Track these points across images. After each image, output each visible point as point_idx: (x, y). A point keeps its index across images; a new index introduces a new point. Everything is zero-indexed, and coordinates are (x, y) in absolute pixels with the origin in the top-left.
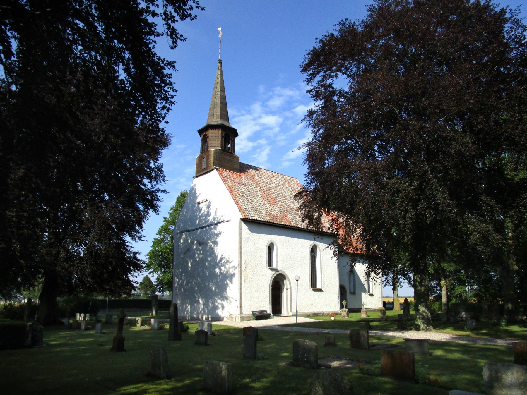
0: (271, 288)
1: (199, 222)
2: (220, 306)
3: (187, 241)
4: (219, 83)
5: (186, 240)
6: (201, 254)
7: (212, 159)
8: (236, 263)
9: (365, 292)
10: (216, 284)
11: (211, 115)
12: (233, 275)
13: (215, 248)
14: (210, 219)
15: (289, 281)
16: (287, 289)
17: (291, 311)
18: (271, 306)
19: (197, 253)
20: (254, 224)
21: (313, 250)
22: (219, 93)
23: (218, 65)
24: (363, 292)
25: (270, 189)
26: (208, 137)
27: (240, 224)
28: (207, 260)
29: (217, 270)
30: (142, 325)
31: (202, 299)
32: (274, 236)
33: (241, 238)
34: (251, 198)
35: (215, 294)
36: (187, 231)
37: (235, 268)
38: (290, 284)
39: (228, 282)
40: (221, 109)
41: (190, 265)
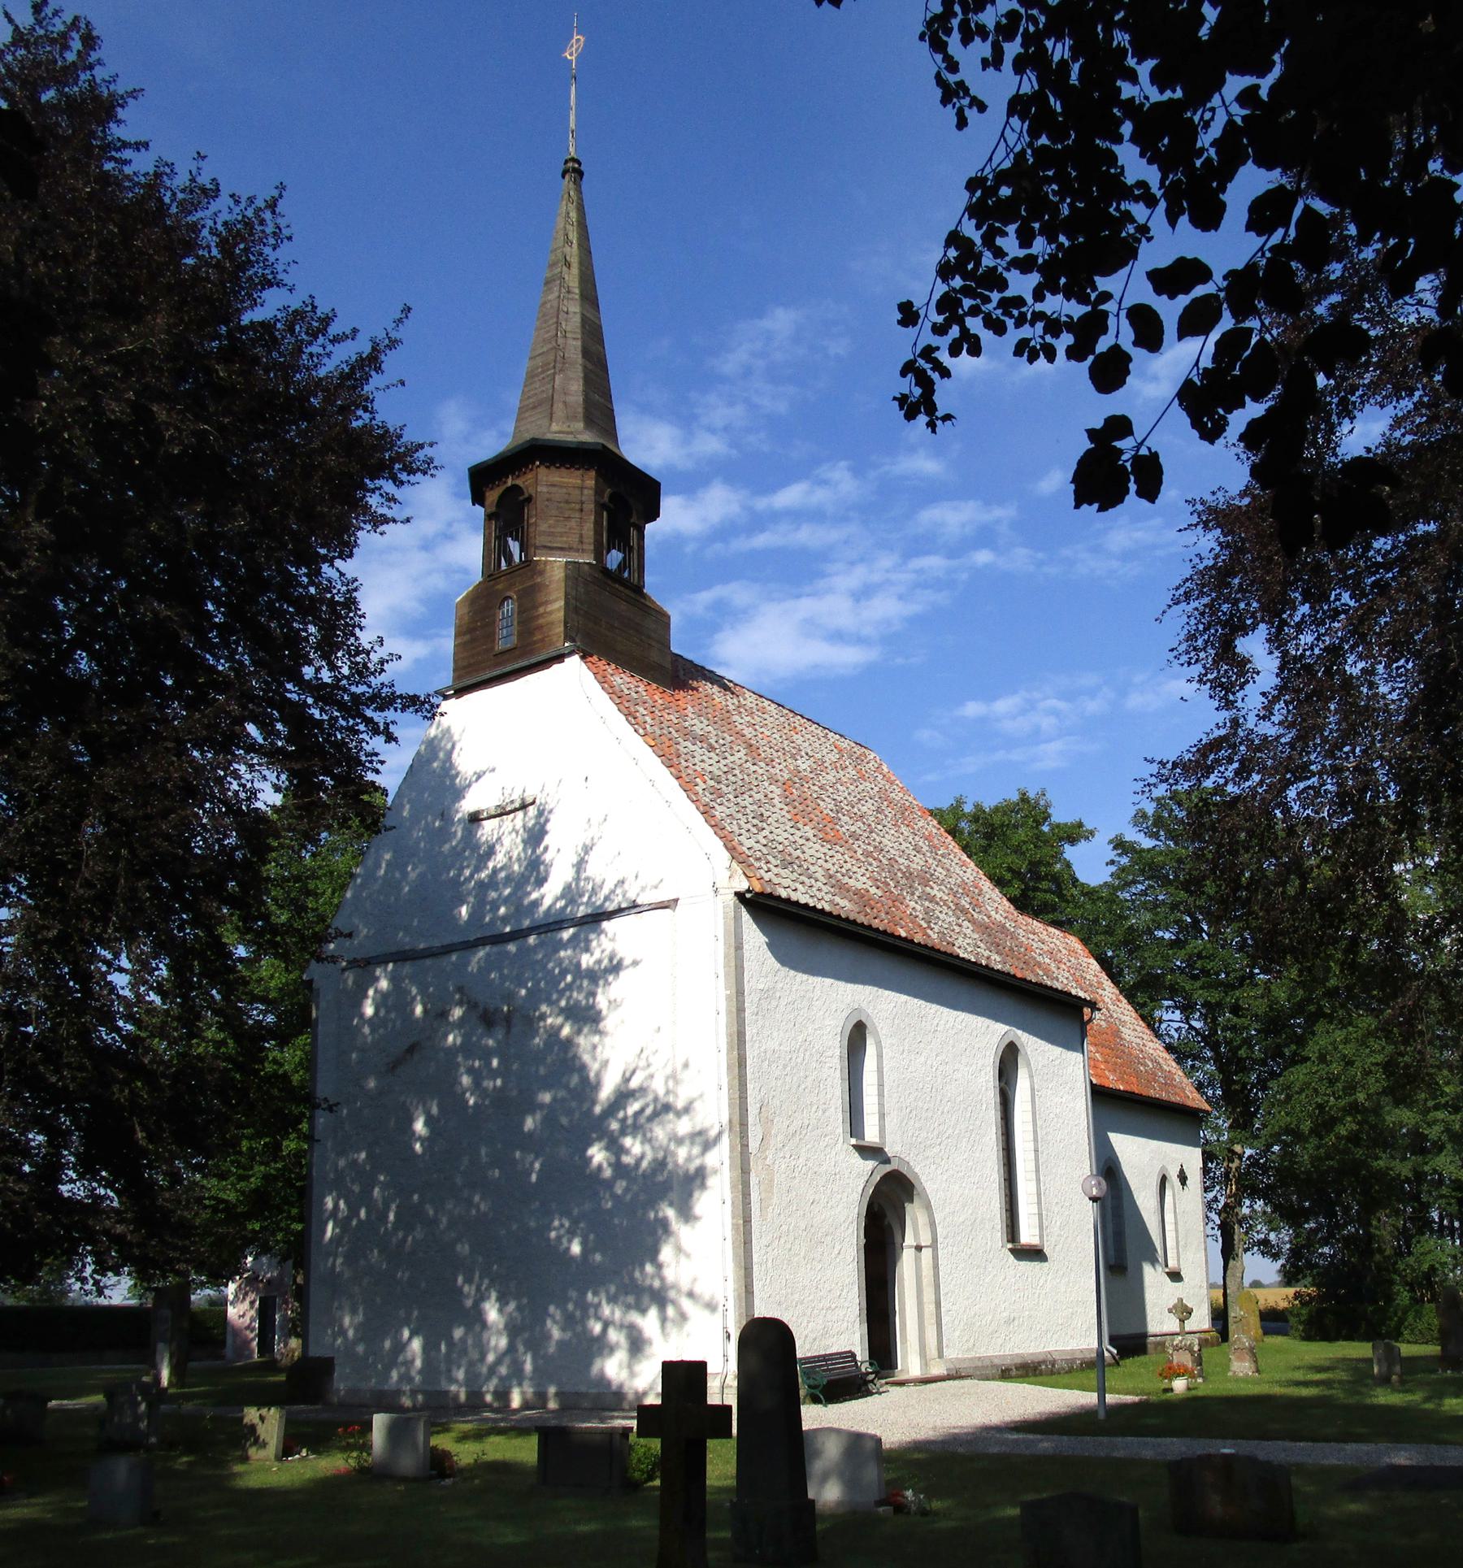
0: (863, 1241)
1: (475, 914)
2: (614, 1335)
3: (405, 1007)
4: (575, 261)
5: (394, 1002)
6: (493, 1074)
7: (555, 608)
8: (713, 1112)
9: (1154, 1261)
10: (597, 1228)
11: (540, 403)
12: (697, 1178)
13: (582, 1041)
14: (549, 894)
15: (928, 1207)
16: (919, 1248)
17: (941, 1355)
19: (471, 1071)
20: (792, 924)
21: (1008, 1062)
22: (575, 308)
23: (567, 183)
24: (1146, 1260)
27: (737, 919)
28: (532, 1107)
29: (598, 1155)
30: (287, 1450)
31: (502, 1300)
32: (869, 989)
33: (740, 993)
35: (587, 1277)
36: (401, 957)
37: (708, 1146)
38: (933, 1224)
39: (670, 1213)
40: (587, 380)
41: (419, 1126)
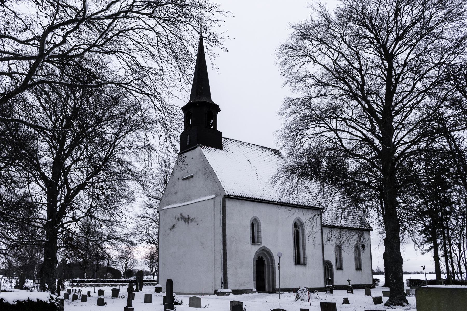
18: (255, 282)
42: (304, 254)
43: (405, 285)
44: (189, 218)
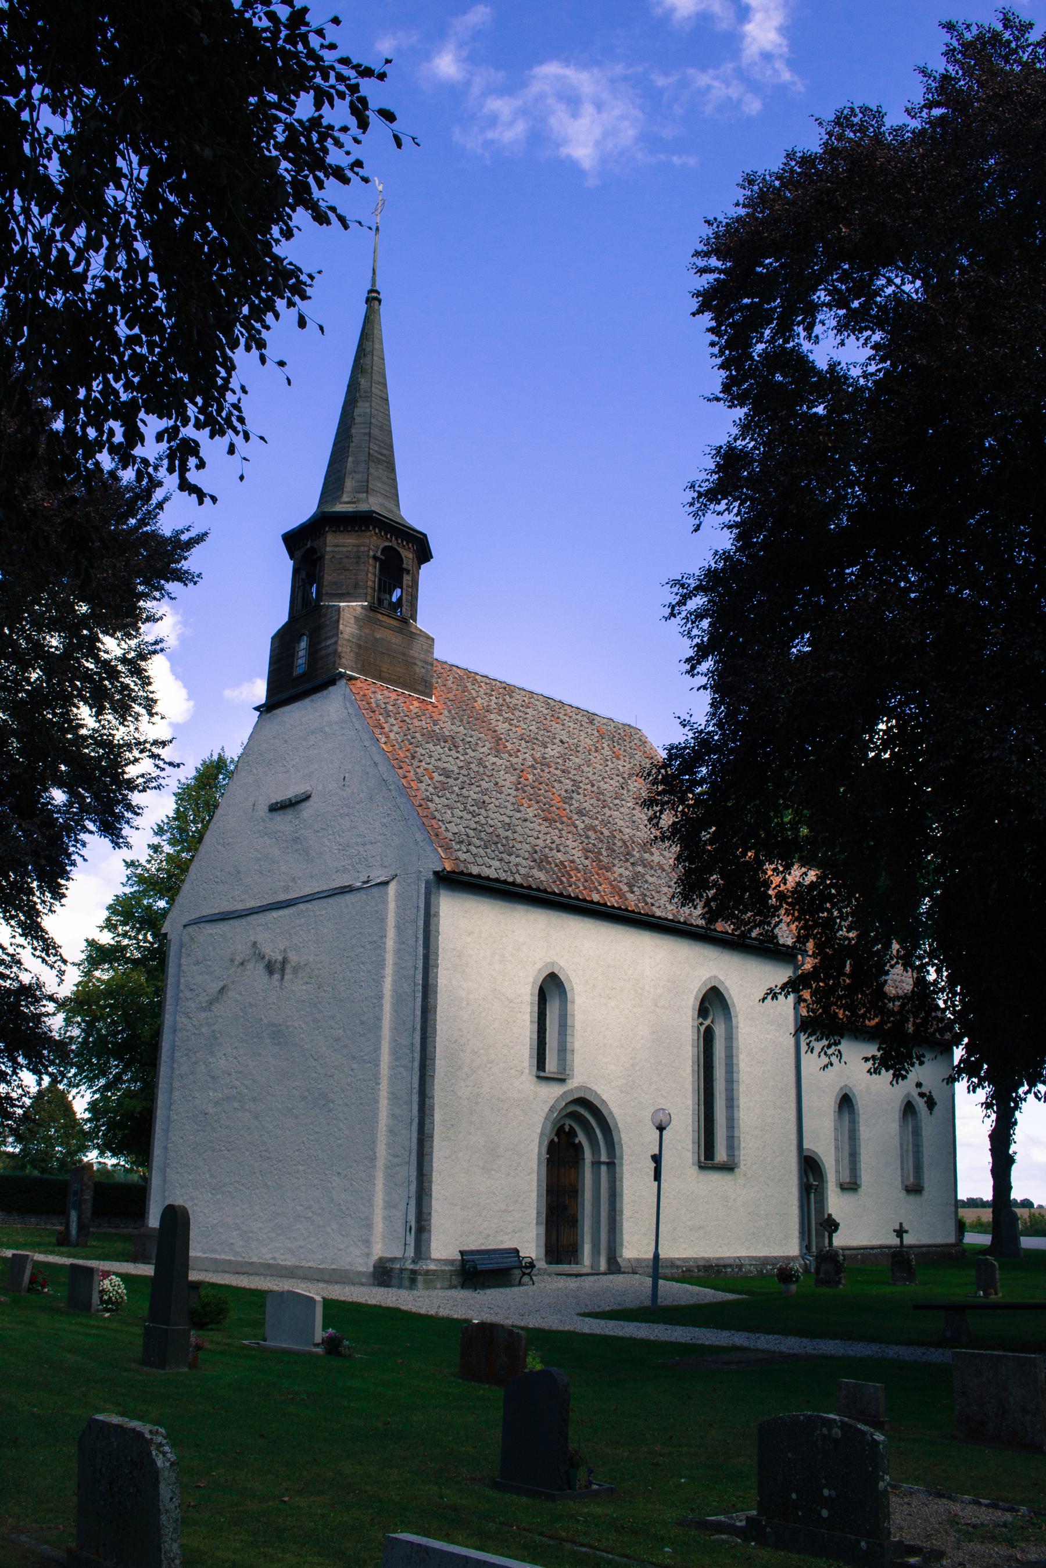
18: (542, 1229)
25: (544, 762)
26: (321, 558)
34: (473, 793)
42: (731, 1123)
43: (154, 1256)
44: (285, 961)
